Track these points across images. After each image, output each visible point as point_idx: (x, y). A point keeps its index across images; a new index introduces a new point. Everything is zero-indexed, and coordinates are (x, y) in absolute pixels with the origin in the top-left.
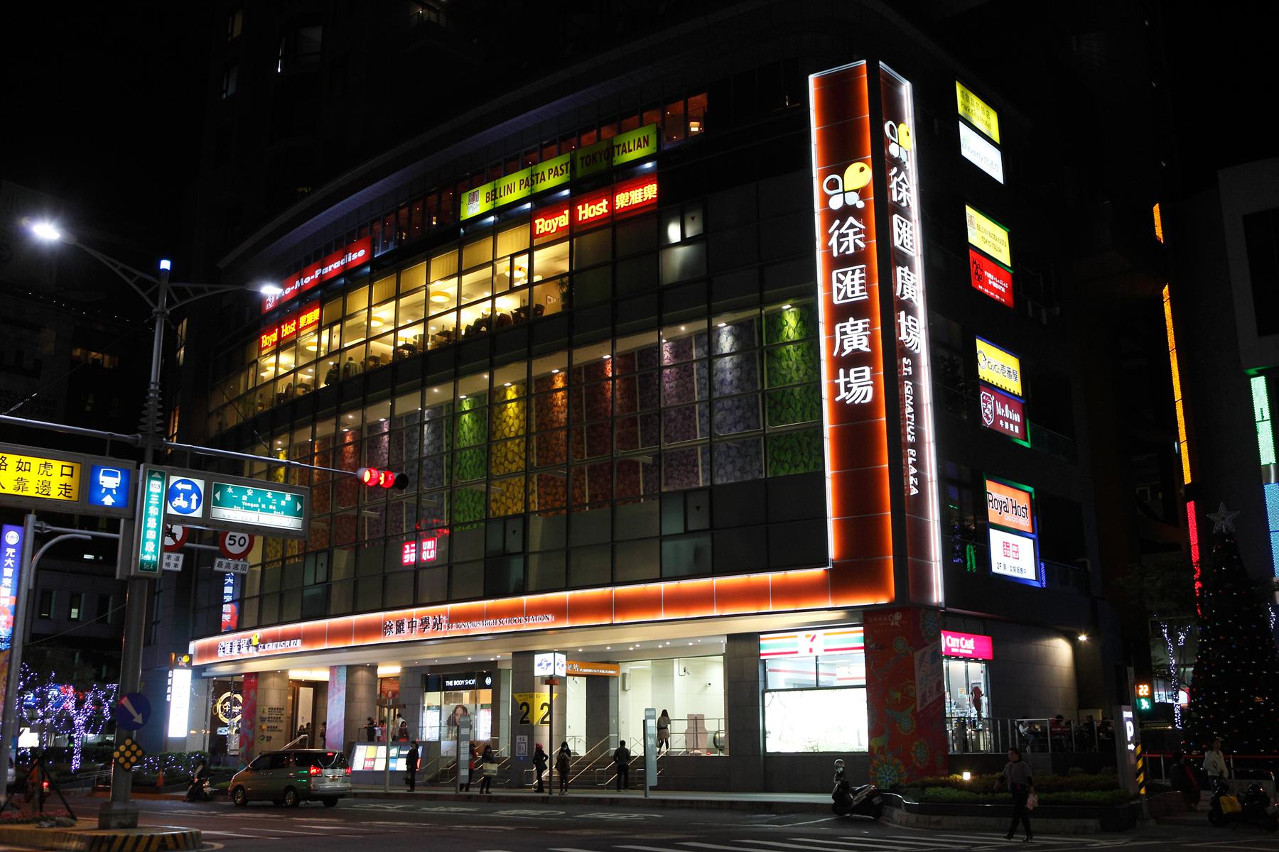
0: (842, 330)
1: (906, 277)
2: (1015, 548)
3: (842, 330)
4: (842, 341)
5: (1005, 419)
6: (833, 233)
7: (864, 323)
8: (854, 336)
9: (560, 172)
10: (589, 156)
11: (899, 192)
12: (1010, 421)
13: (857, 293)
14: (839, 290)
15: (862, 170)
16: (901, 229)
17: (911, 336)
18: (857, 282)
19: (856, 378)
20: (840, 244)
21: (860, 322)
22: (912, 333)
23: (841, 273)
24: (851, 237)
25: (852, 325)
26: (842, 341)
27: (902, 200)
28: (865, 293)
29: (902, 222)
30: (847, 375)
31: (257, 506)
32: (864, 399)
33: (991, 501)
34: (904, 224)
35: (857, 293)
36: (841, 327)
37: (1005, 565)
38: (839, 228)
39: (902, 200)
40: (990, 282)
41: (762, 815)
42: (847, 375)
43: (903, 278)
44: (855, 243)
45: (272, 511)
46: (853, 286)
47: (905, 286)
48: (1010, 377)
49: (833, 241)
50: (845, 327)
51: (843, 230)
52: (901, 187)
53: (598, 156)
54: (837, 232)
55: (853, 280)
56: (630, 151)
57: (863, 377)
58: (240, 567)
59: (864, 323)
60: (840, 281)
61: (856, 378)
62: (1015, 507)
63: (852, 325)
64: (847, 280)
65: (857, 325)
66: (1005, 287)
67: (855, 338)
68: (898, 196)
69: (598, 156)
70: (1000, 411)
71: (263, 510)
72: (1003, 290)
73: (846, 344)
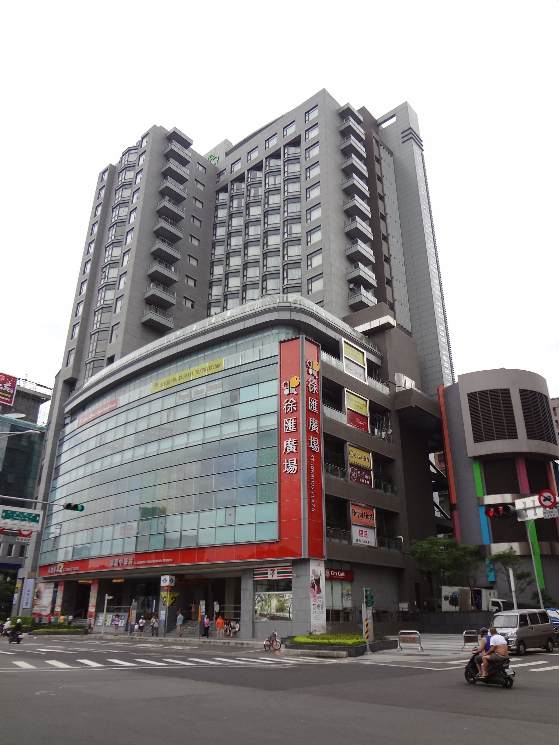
0: (287, 443)
1: (313, 422)
2: (366, 533)
3: (287, 443)
4: (286, 447)
5: (362, 478)
6: (285, 404)
7: (295, 441)
8: (291, 446)
9: (188, 376)
10: (199, 370)
11: (312, 388)
12: (365, 479)
13: (293, 428)
14: (286, 427)
15: (297, 379)
16: (312, 402)
17: (314, 445)
18: (293, 424)
19: (291, 463)
20: (287, 409)
21: (293, 440)
22: (315, 444)
23: (287, 420)
24: (292, 406)
25: (290, 441)
26: (286, 447)
27: (313, 391)
28: (296, 428)
29: (313, 400)
30: (287, 461)
31: (20, 518)
32: (293, 471)
33: (354, 513)
34: (314, 401)
35: (293, 428)
36: (286, 442)
37: (360, 540)
38: (287, 402)
39: (313, 391)
40: (357, 422)
41: (39, 653)
42: (287, 461)
43: (312, 422)
44: (293, 408)
45: (26, 520)
46: (291, 425)
47: (312, 426)
48: (365, 461)
49: (285, 407)
50: (288, 442)
51: (288, 403)
52: (313, 386)
53: (202, 370)
54: (286, 404)
55: (291, 423)
56: (213, 369)
57: (294, 462)
58: (27, 540)
59: (295, 441)
60: (286, 423)
61: (291, 463)
62: (366, 515)
63: (290, 441)
64: (289, 423)
65: (292, 441)
66: (364, 424)
67: (291, 447)
68: (311, 389)
69: (202, 370)
70: (360, 475)
71: (22, 520)
72: (363, 425)
73: (288, 449)
